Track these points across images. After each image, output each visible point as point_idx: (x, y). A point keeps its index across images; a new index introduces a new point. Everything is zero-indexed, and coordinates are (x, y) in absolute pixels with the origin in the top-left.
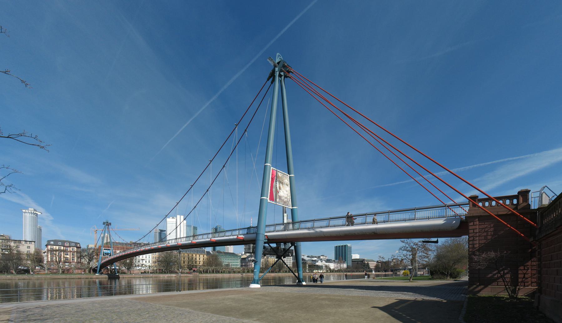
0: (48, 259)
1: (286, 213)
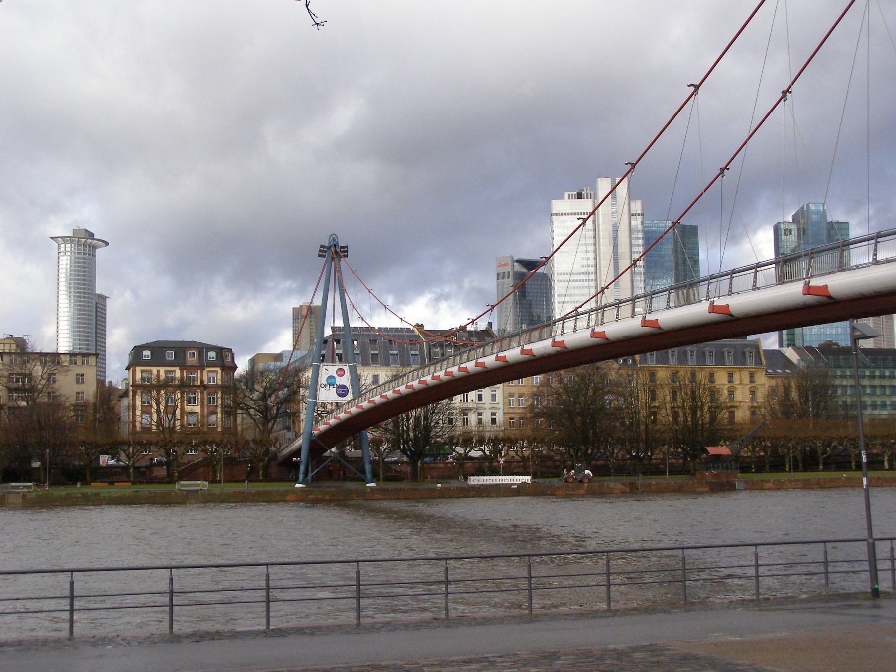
0: (731, 466)
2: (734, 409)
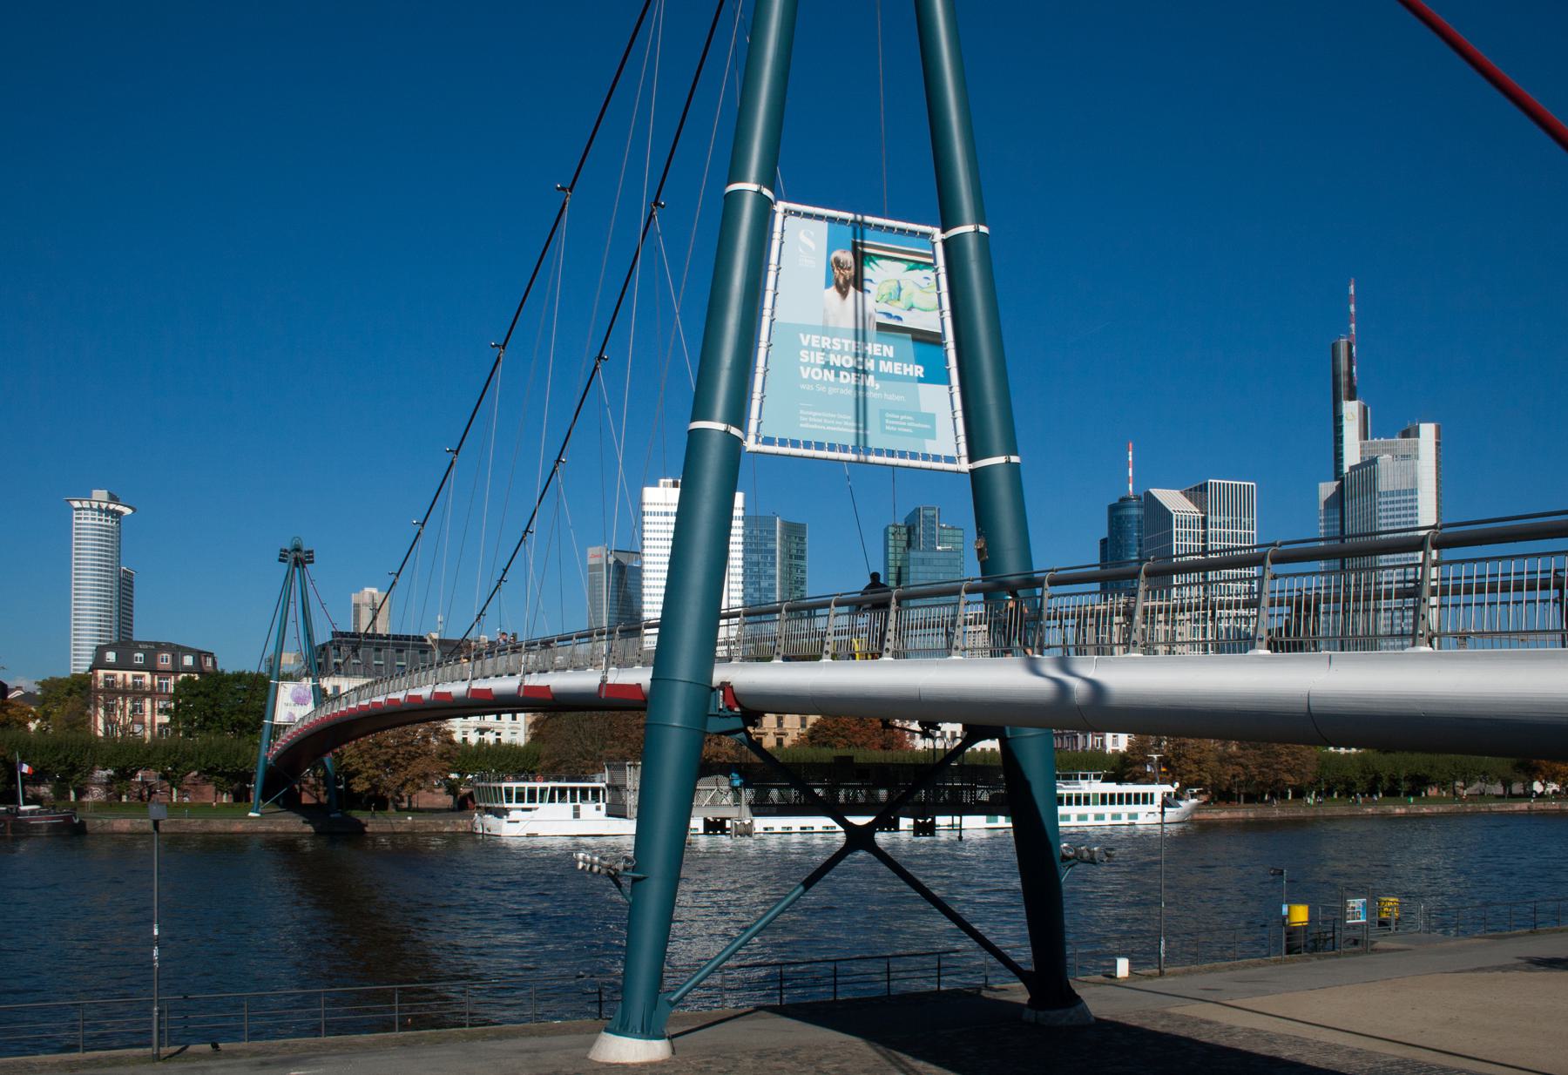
1: (1351, 398)
2: (763, 736)
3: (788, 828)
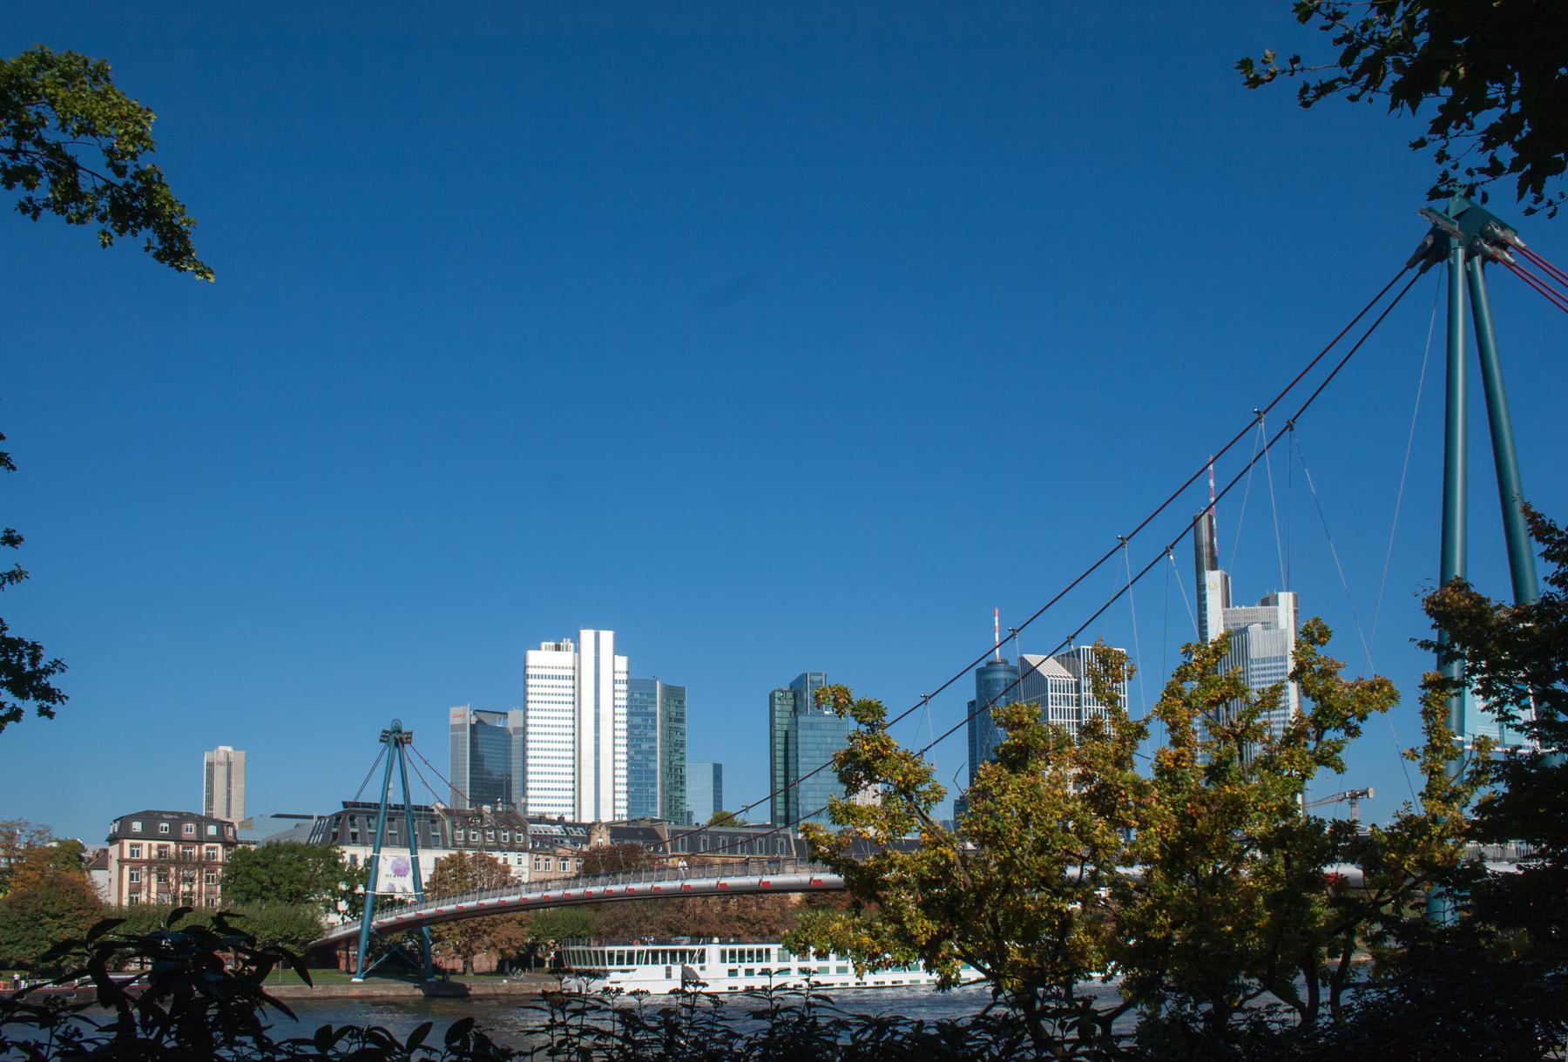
1: (1213, 567)
3: (845, 984)
